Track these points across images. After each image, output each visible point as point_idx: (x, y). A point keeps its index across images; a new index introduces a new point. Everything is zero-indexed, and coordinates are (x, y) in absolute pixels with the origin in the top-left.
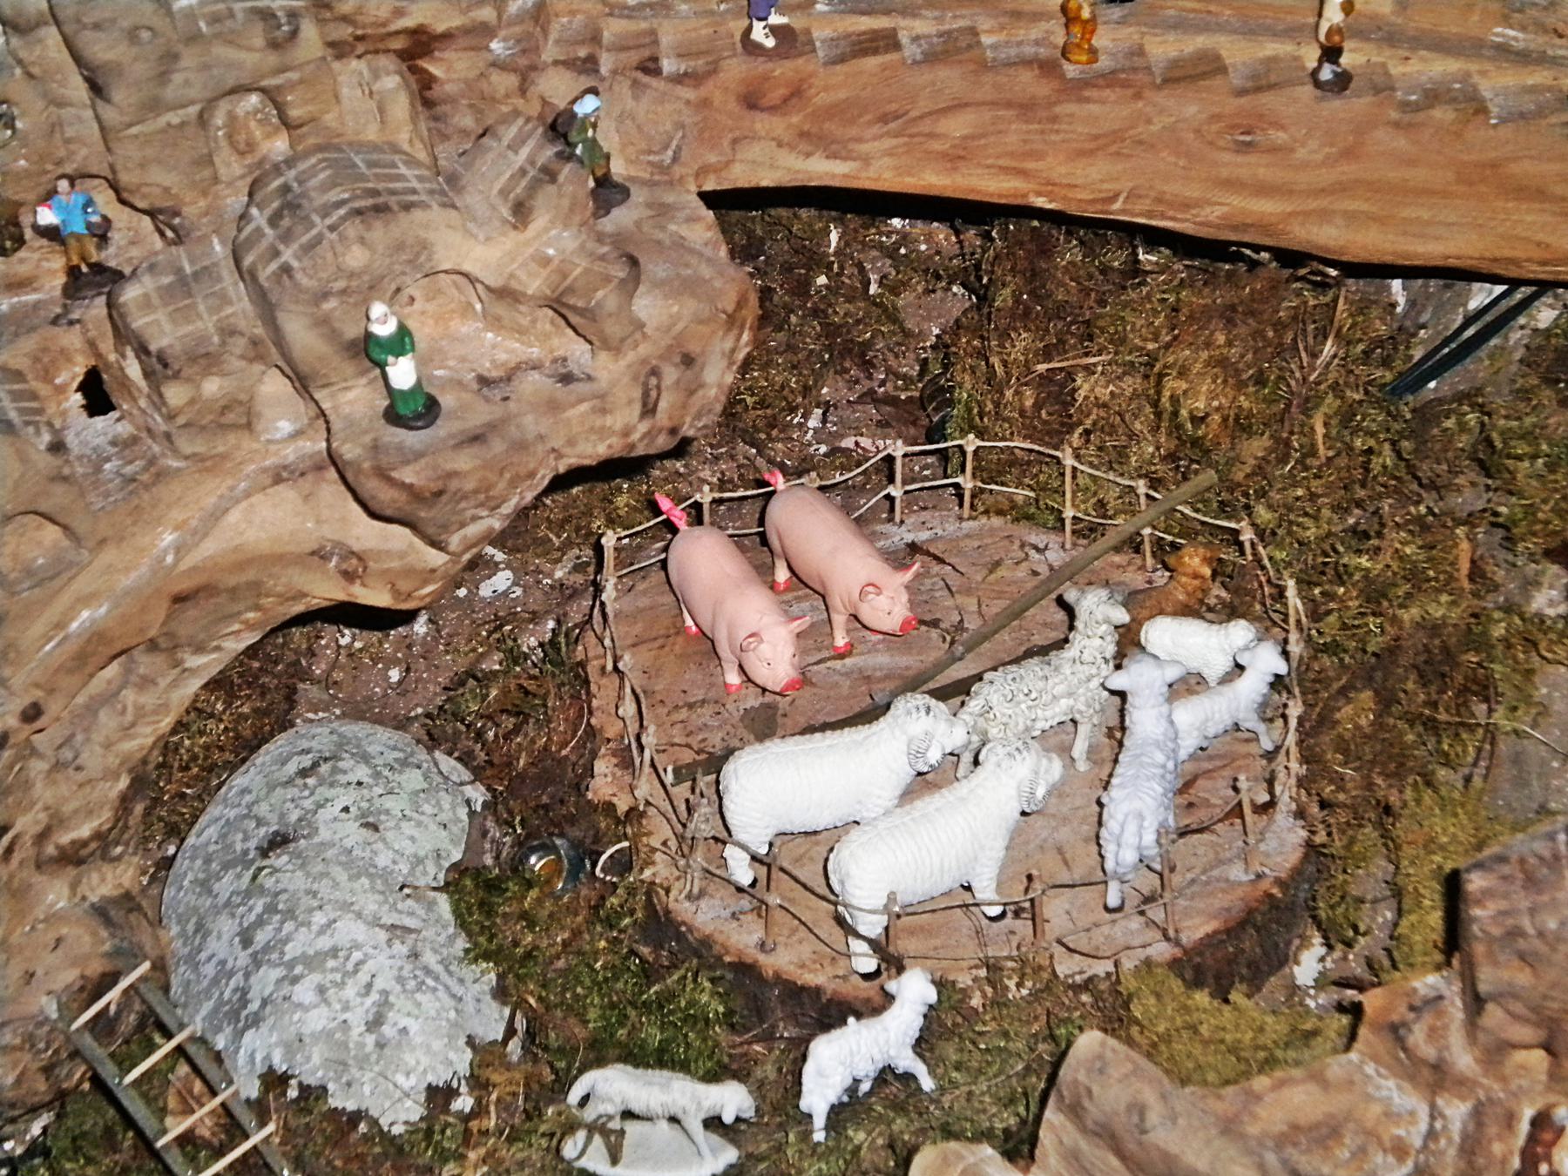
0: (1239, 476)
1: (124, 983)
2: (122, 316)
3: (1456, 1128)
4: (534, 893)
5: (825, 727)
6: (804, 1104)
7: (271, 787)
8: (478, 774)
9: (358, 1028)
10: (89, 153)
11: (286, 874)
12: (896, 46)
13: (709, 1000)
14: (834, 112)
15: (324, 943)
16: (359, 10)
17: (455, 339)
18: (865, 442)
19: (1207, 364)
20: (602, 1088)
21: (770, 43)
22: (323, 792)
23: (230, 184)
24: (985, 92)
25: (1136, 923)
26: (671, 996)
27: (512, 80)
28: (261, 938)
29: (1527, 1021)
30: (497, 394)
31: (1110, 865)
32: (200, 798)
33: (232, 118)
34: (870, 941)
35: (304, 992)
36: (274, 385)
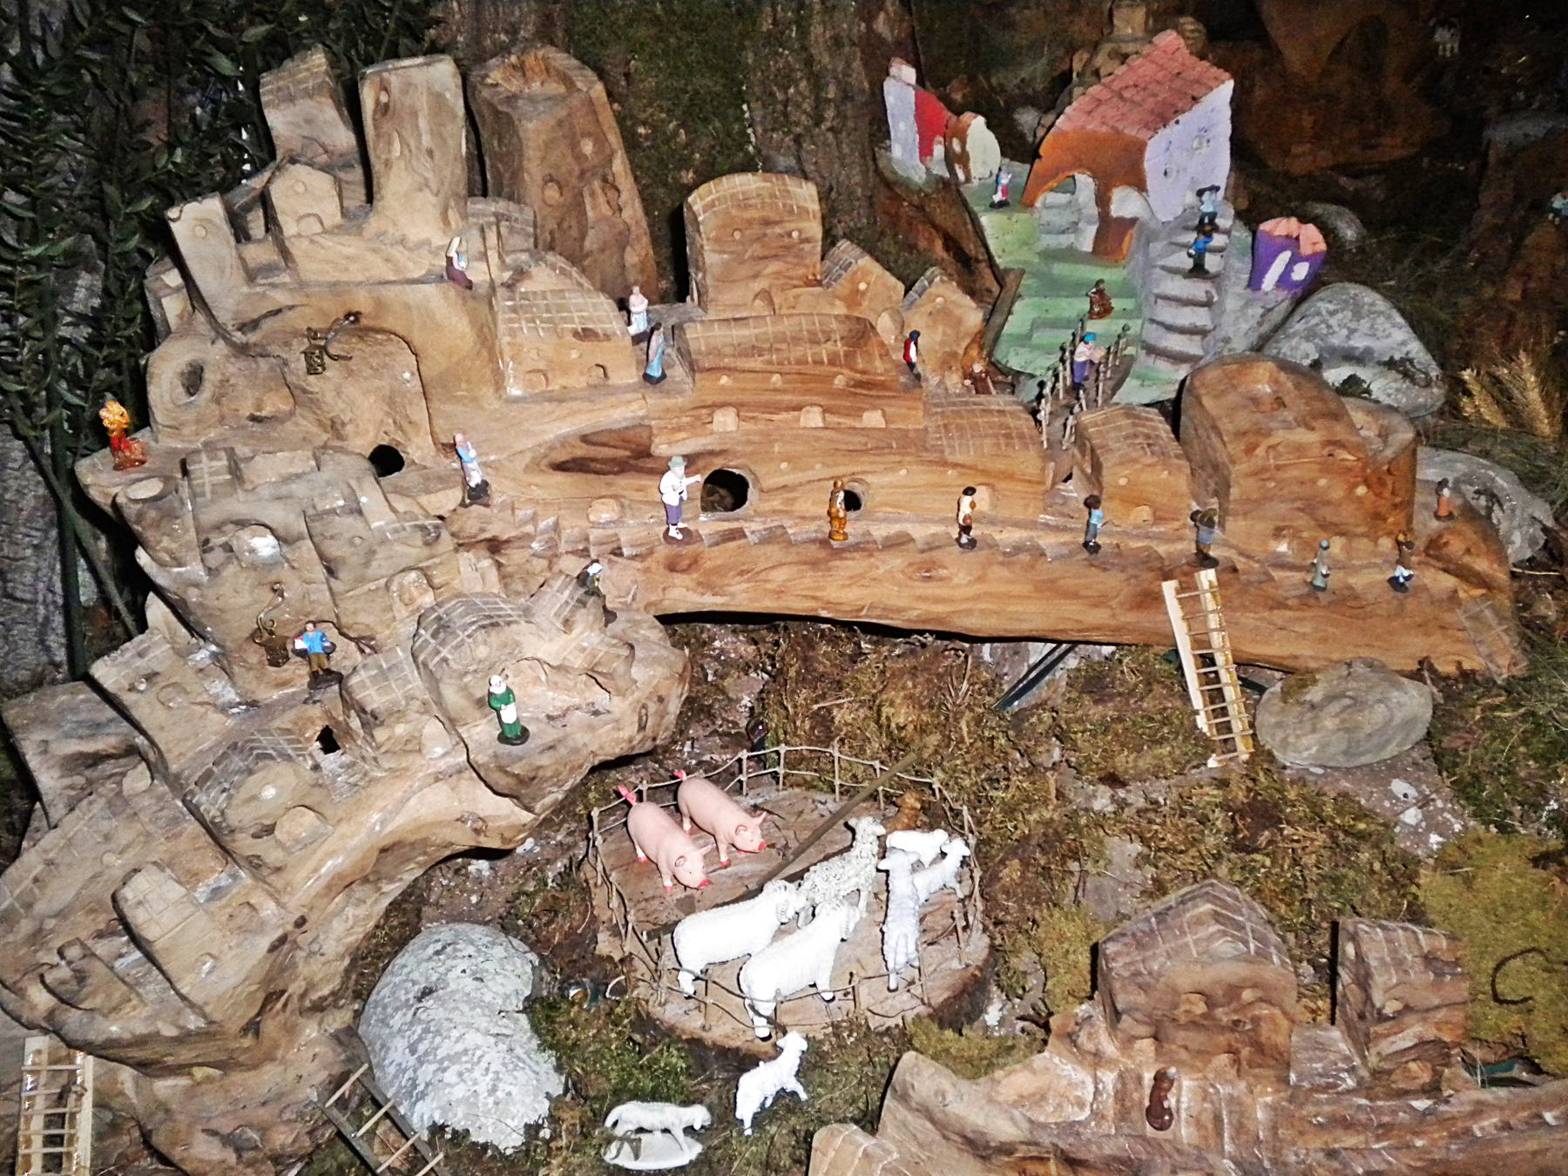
0: (926, 756)
1: (353, 1078)
2: (350, 694)
3: (1110, 1087)
4: (576, 1008)
5: (727, 903)
6: (739, 1115)
7: (419, 963)
8: (533, 947)
9: (483, 1094)
10: (324, 608)
11: (433, 1009)
12: (745, 536)
13: (677, 1061)
14: (719, 571)
15: (459, 1047)
16: (461, 529)
17: (530, 697)
18: (715, 757)
19: (905, 698)
20: (624, 1116)
21: (680, 537)
22: (450, 963)
23: (402, 621)
24: (792, 557)
25: (906, 996)
26: (656, 1061)
27: (545, 563)
28: (422, 1048)
29: (1145, 1023)
30: (559, 723)
31: (891, 965)
32: (373, 974)
33: (401, 585)
34: (768, 1018)
35: (450, 1076)
36: (433, 728)
